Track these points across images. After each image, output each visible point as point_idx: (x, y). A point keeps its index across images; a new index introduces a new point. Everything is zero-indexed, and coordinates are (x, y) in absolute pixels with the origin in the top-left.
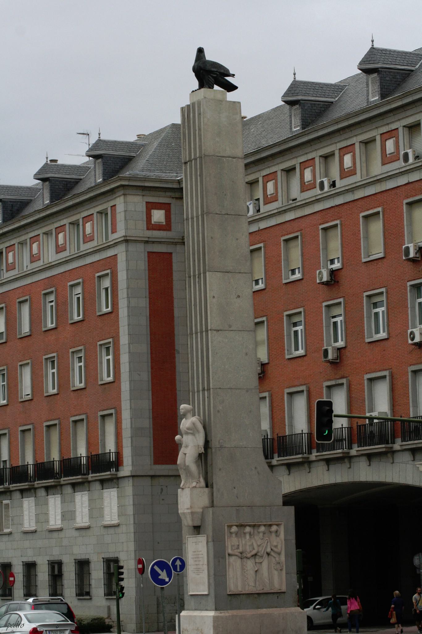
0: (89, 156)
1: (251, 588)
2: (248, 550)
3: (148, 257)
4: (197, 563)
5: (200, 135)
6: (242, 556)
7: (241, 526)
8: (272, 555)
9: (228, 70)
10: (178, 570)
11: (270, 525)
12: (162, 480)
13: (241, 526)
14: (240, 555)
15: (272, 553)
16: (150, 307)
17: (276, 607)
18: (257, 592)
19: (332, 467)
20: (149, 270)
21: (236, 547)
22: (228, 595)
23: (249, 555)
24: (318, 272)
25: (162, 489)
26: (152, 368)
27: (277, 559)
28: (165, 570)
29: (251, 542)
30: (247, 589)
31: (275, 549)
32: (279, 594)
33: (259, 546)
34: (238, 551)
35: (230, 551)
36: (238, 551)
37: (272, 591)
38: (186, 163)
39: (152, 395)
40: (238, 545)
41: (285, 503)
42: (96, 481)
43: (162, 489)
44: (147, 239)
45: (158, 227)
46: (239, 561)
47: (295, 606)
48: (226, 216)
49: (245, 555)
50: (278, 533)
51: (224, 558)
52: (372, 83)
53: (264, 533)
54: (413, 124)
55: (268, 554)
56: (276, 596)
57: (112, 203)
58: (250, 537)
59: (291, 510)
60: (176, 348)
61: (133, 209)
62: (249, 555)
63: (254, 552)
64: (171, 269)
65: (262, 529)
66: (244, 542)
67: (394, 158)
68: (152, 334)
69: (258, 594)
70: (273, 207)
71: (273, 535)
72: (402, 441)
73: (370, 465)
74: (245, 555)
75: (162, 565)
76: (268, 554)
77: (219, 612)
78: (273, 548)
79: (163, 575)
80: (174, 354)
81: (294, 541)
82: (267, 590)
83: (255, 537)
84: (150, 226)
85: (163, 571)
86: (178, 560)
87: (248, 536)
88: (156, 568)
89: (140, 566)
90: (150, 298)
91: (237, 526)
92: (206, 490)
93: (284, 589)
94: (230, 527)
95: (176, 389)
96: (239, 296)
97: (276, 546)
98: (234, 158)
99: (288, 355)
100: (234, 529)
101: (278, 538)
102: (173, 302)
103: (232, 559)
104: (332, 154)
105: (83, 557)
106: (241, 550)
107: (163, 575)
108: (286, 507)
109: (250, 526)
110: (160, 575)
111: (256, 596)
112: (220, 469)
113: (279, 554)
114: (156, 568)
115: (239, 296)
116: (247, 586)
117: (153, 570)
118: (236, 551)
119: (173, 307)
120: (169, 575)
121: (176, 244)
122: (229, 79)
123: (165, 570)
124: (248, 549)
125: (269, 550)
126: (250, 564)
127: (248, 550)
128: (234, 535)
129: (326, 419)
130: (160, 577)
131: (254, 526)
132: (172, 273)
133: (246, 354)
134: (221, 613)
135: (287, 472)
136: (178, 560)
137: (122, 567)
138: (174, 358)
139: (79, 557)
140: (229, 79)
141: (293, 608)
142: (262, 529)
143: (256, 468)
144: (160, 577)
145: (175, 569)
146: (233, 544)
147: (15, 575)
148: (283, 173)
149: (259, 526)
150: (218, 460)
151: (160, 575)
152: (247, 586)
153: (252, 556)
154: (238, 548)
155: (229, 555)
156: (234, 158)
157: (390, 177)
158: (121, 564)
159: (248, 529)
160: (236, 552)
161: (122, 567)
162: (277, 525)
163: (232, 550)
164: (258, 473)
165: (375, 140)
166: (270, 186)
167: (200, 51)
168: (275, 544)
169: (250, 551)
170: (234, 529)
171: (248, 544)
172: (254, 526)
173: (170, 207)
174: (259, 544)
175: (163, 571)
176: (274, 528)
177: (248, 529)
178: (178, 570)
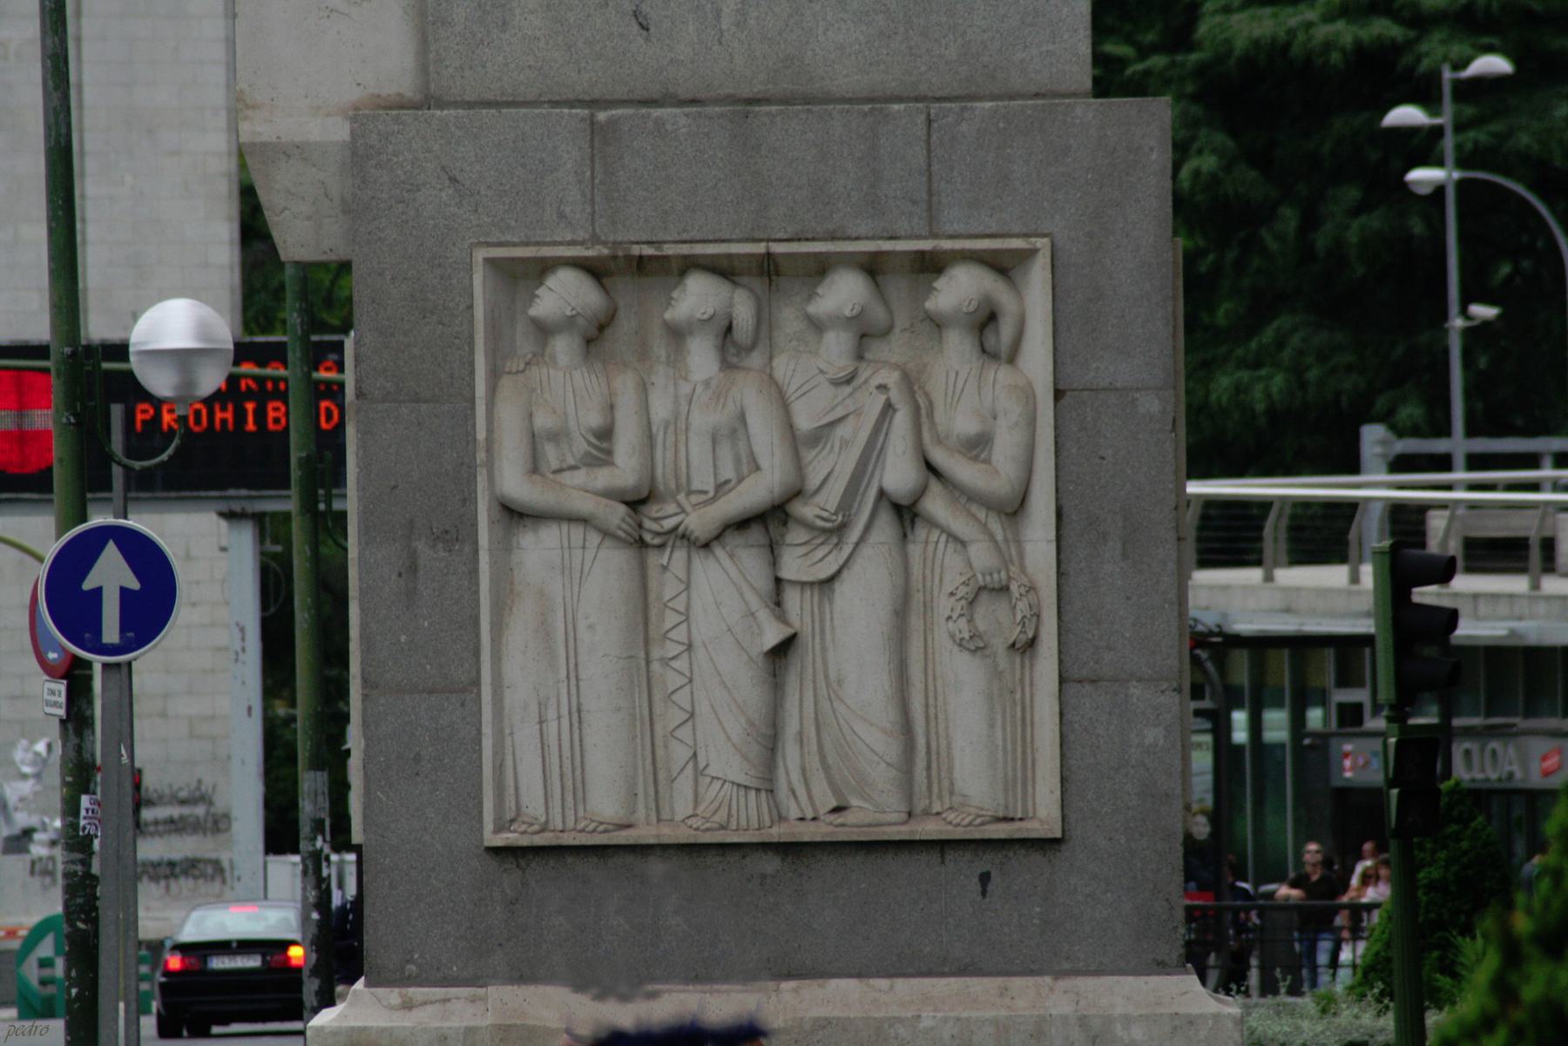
1: (710, 791)
2: (703, 480)
8: (932, 523)
11: (930, 266)
13: (627, 271)
14: (616, 514)
15: (936, 504)
17: (964, 970)
18: (777, 833)
21: (581, 446)
22: (496, 851)
27: (982, 555)
28: (87, 585)
29: (793, 398)
30: (682, 808)
31: (963, 471)
32: (993, 852)
33: (797, 443)
34: (603, 478)
35: (515, 484)
36: (603, 478)
37: (929, 829)
40: (605, 434)
46: (608, 568)
47: (1161, 967)
49: (663, 516)
50: (1006, 330)
51: (458, 535)
53: (865, 335)
55: (906, 513)
56: (966, 869)
58: (726, 365)
62: (700, 521)
63: (753, 494)
65: (844, 292)
66: (660, 409)
69: (789, 850)
71: (958, 344)
76: (906, 513)
77: (393, 995)
78: (939, 457)
82: (877, 812)
83: (782, 367)
86: (111, 552)
87: (702, 357)
91: (595, 270)
93: (1044, 816)
97: (978, 446)
99: (287, 517)
100: (564, 294)
101: (1003, 374)
103: (538, 550)
106: (625, 470)
109: (725, 270)
110: (124, 592)
111: (770, 864)
113: (1014, 509)
116: (684, 786)
118: (579, 477)
123: (87, 585)
125: (898, 474)
126: (718, 600)
127: (703, 480)
128: (564, 347)
131: (768, 271)
134: (408, 1006)
136: (111, 552)
141: (1129, 982)
142: (844, 292)
146: (543, 421)
149: (820, 268)
151: (124, 592)
152: (684, 786)
153: (742, 524)
155: (514, 515)
159: (698, 296)
160: (580, 490)
162: (1003, 266)
163: (535, 467)
168: (965, 425)
169: (721, 487)
170: (564, 294)
171: (703, 419)
172: (768, 271)
174: (805, 422)
176: (959, 288)
177: (698, 296)
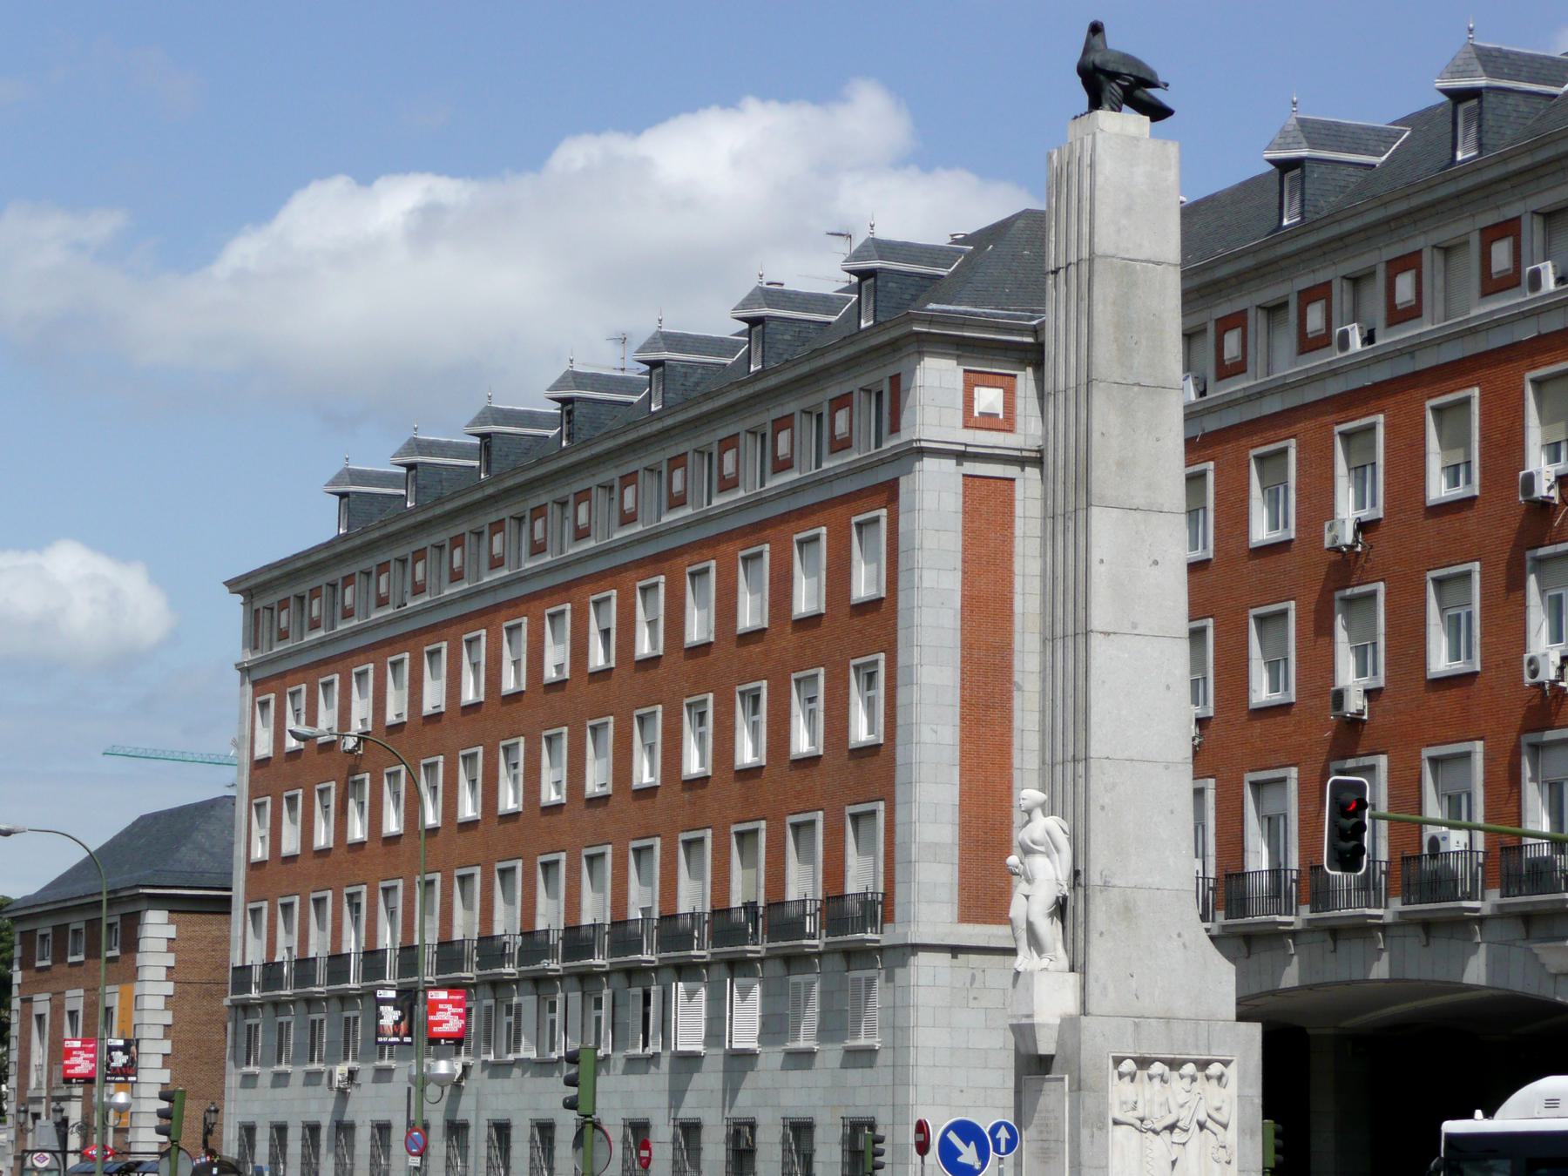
0: (851, 272)
3: (965, 485)
4: (1045, 1136)
5: (1092, 213)
6: (1142, 1126)
7: (1143, 1063)
9: (1153, 74)
10: (1003, 1149)
11: (1207, 1063)
12: (974, 959)
13: (1143, 1063)
14: (1138, 1123)
15: (1210, 1124)
16: (963, 590)
19: (1343, 946)
20: (965, 512)
21: (1131, 1105)
23: (1158, 1127)
24: (1327, 525)
25: (973, 977)
26: (962, 719)
38: (1055, 272)
39: (961, 776)
41: (1241, 1017)
42: (833, 952)
43: (973, 977)
44: (962, 448)
45: (988, 422)
48: (1136, 389)
49: (1148, 1124)
52: (1467, 121)
54: (1553, 208)
55: (1202, 1126)
57: (892, 371)
59: (1254, 1031)
60: (1017, 677)
61: (936, 384)
63: (1169, 1121)
64: (1012, 513)
67: (1509, 282)
68: (963, 887)
70: (1237, 386)
72: (1502, 896)
73: (1427, 945)
74: (1148, 1124)
75: (967, 1130)
79: (969, 1155)
80: (1010, 692)
81: (1258, 1101)
84: (970, 422)
85: (967, 1145)
88: (952, 1136)
89: (921, 1137)
90: (964, 572)
92: (1074, 978)
94: (1118, 1061)
95: (1010, 766)
96: (1156, 563)
97: (1218, 1109)
98: (1158, 263)
100: (1128, 1066)
102: (1011, 583)
104: (1370, 274)
105: (801, 1114)
107: (969, 1155)
108: (1243, 1025)
110: (960, 1154)
112: (1101, 934)
114: (952, 1136)
115: (1156, 563)
117: (944, 1141)
119: (1011, 592)
120: (983, 1156)
121: (1022, 462)
122: (1155, 93)
124: (1157, 1112)
125: (1202, 1117)
126: (1160, 1144)
129: (1349, 823)
130: (960, 1159)
132: (1013, 521)
133: (1168, 687)
135: (1244, 950)
137: (881, 1140)
138: (1010, 699)
139: (792, 1114)
140: (1155, 93)
142: (1189, 1069)
143: (1179, 935)
144: (960, 1159)
145: (997, 1150)
147: (654, 1147)
148: (1260, 312)
150: (1100, 913)
151: (960, 1154)
154: (1134, 1109)
155: (1116, 1123)
156: (1158, 263)
157: (1499, 323)
158: (880, 1132)
160: (1130, 1117)
161: (881, 1140)
162: (1226, 1063)
164: (1184, 946)
165: (1467, 243)
166: (1232, 341)
167: (1096, 29)
170: (1128, 1066)
173: (1012, 490)
175: (967, 1145)
176: (1215, 1069)
178: (1003, 1149)
